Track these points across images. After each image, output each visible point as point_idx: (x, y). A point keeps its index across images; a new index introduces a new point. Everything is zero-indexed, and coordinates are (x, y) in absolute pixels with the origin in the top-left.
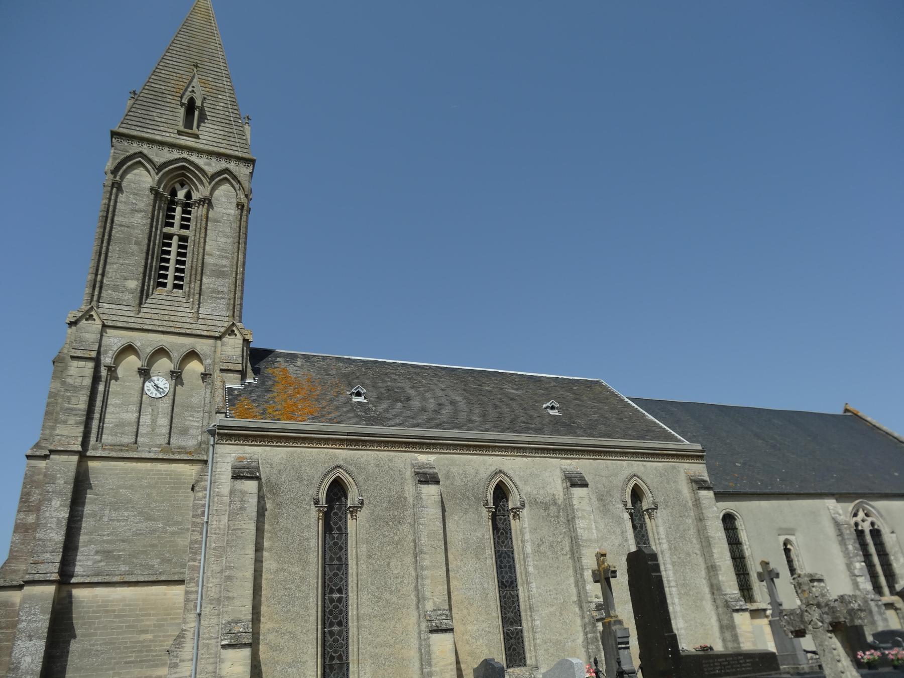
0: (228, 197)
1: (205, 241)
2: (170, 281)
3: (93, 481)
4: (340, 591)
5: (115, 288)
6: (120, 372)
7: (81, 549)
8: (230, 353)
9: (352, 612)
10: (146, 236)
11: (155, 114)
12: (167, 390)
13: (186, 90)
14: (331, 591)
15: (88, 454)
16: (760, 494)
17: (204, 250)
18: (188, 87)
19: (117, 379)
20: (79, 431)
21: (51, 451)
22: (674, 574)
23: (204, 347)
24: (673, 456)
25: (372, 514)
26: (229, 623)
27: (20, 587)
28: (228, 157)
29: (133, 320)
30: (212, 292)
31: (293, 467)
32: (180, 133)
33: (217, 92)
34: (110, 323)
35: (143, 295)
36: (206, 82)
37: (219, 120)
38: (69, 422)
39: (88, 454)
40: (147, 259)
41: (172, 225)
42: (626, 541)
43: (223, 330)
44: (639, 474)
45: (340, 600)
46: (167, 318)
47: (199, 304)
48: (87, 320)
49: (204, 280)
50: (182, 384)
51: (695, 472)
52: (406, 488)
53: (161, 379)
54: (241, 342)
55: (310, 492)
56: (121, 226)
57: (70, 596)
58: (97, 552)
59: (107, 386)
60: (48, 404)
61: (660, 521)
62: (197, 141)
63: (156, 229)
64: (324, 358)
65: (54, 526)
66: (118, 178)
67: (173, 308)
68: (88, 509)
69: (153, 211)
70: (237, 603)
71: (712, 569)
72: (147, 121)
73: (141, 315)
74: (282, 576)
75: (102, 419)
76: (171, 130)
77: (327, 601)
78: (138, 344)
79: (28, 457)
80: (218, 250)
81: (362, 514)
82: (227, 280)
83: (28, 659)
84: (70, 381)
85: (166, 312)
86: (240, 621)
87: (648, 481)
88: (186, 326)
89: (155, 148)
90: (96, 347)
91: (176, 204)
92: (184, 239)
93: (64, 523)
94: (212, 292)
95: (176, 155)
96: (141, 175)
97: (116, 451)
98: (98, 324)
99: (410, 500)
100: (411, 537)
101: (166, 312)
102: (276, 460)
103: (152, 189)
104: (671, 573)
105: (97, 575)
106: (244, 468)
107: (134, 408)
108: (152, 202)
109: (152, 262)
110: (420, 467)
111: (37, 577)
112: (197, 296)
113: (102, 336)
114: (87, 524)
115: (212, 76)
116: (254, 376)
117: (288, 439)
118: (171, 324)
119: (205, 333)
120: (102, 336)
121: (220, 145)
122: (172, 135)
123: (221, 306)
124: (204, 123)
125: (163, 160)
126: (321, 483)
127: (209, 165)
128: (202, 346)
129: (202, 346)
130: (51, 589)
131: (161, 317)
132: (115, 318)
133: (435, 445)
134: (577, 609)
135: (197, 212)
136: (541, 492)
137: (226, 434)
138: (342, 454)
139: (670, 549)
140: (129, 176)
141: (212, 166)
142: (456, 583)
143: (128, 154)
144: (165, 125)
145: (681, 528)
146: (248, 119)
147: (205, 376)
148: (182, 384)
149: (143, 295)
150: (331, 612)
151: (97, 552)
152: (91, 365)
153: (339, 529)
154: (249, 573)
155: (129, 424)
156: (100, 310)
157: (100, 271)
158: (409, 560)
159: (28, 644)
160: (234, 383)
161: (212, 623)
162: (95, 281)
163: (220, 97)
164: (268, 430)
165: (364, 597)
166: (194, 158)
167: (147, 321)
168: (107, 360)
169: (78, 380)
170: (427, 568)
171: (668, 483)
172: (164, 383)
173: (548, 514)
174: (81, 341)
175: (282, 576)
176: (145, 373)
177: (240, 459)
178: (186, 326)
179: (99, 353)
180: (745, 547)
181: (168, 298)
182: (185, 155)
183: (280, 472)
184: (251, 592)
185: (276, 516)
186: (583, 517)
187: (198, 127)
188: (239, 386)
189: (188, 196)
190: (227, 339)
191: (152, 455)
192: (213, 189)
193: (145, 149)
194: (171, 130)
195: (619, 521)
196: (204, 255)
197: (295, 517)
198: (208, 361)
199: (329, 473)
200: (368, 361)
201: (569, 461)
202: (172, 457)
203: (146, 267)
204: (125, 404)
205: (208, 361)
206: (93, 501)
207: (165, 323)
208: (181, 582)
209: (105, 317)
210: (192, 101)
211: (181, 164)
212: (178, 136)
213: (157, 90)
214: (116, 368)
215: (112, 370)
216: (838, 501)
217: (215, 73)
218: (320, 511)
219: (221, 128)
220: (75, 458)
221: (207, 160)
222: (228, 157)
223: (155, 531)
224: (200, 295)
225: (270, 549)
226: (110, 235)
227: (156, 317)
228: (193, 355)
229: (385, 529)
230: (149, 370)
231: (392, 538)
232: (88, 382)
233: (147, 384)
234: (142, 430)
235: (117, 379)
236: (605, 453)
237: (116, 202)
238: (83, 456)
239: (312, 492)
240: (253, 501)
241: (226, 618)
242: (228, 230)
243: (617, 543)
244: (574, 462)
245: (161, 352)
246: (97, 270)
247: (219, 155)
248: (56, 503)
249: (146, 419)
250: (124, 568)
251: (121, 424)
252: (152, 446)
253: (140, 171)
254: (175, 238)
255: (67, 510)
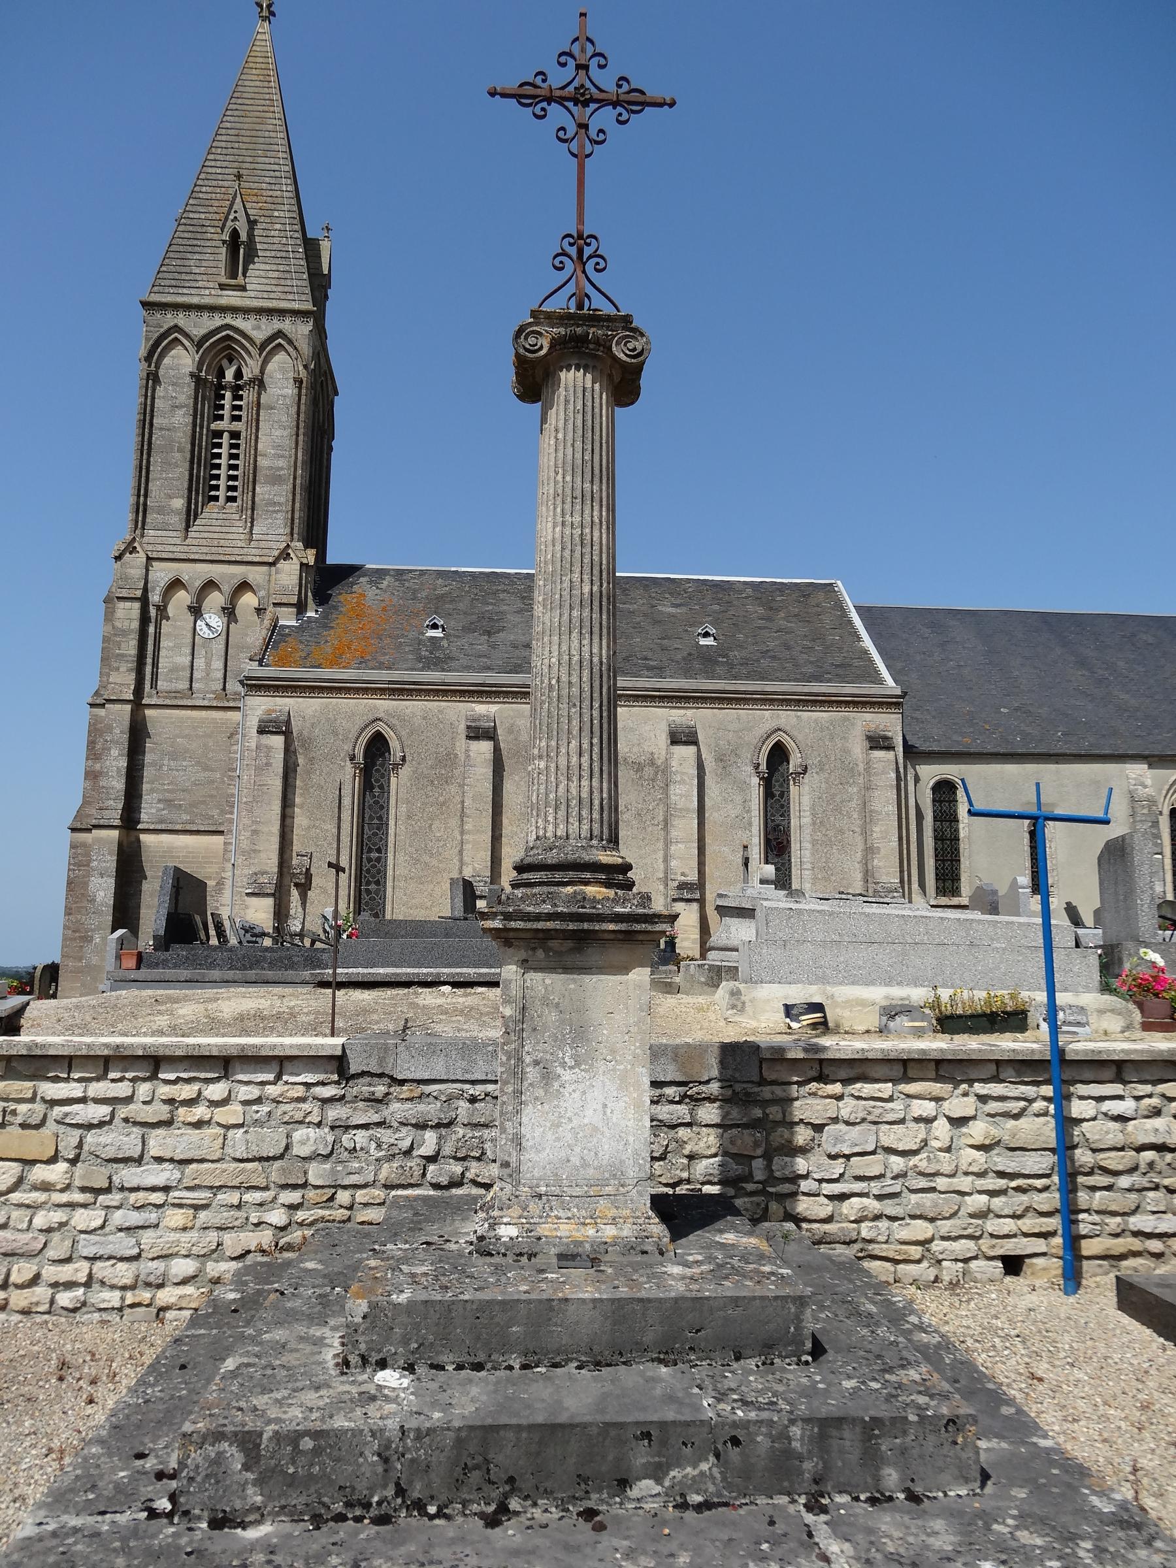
0: (283, 370)
1: (257, 437)
2: (221, 493)
3: (151, 731)
4: (379, 851)
5: (161, 510)
6: (171, 610)
7: (144, 797)
8: (286, 583)
9: (390, 873)
10: (189, 440)
11: (192, 263)
12: (220, 629)
13: (226, 219)
14: (370, 850)
15: (144, 702)
16: (992, 754)
17: (256, 449)
18: (229, 213)
19: (168, 618)
20: (131, 678)
21: (109, 701)
22: (813, 854)
23: (257, 577)
24: (847, 703)
25: (414, 772)
26: (256, 874)
27: (88, 830)
28: (281, 313)
29: (179, 548)
30: (267, 505)
31: (328, 720)
32: (222, 287)
33: (273, 206)
34: (155, 555)
35: (191, 516)
36: (259, 192)
37: (273, 253)
38: (121, 669)
39: (144, 702)
40: (191, 469)
41: (221, 418)
42: (749, 811)
43: (276, 553)
44: (788, 728)
45: (378, 860)
46: (216, 543)
47: (252, 523)
48: (131, 553)
49: (258, 489)
50: (236, 621)
51: (878, 726)
52: (458, 744)
53: (213, 616)
54: (298, 567)
55: (346, 747)
56: (161, 429)
57: (139, 840)
58: (160, 801)
59: (158, 627)
60: (103, 649)
61: (806, 789)
62: (244, 294)
63: (202, 427)
64: (423, 573)
65: (115, 774)
66: (153, 367)
67: (224, 529)
68: (148, 758)
69: (196, 403)
70: (263, 855)
71: (869, 851)
72: (183, 276)
73: (188, 541)
74: (313, 832)
75: (155, 664)
76: (211, 285)
77: (364, 860)
78: (185, 578)
79: (92, 705)
80: (274, 448)
81: (405, 772)
82: (285, 487)
83: (102, 894)
84: (118, 624)
85: (216, 536)
86: (266, 873)
87: (800, 737)
88: (236, 551)
89: (193, 314)
90: (142, 584)
91: (224, 388)
92: (235, 435)
93: (124, 771)
94: (267, 505)
95: (218, 321)
96: (178, 357)
97: (170, 698)
98: (141, 558)
99: (462, 757)
100: (458, 799)
101: (216, 536)
102: (310, 712)
103: (192, 375)
104: (807, 854)
105: (161, 822)
106: (271, 721)
107: (188, 651)
108: (192, 392)
109: (198, 471)
110: (474, 720)
111: (102, 822)
112: (249, 512)
113: (147, 570)
114: (148, 773)
115: (267, 180)
116: (315, 607)
117: (322, 689)
118: (220, 550)
119: (257, 559)
120: (147, 570)
121: (272, 295)
122: (213, 292)
123: (278, 522)
124: (254, 263)
125: (203, 332)
126: (357, 739)
127: (258, 328)
128: (255, 575)
129: (255, 575)
130: (115, 834)
131: (209, 542)
132: (160, 548)
133: (497, 694)
134: (661, 887)
135: (248, 395)
136: (635, 750)
137: (254, 685)
138: (383, 705)
139: (814, 823)
140: (166, 361)
141: (258, 329)
142: (509, 850)
143: (162, 330)
144: (205, 277)
145: (838, 799)
146: (328, 229)
147: (259, 611)
148: (236, 621)
149: (191, 516)
150: (368, 871)
151: (160, 801)
152: (137, 605)
153: (381, 787)
154: (276, 828)
155: (183, 669)
156: (145, 540)
157: (142, 492)
158: (454, 822)
159: (100, 880)
160: (288, 620)
161: (244, 871)
162: (138, 503)
163: (276, 214)
164: (298, 680)
165: (401, 858)
166: (239, 323)
167: (194, 549)
168: (155, 598)
169: (126, 623)
170: (469, 832)
171: (832, 739)
172: (215, 620)
173: (641, 777)
174: (127, 579)
175: (313, 832)
176: (196, 611)
177: (269, 712)
178: (236, 551)
179: (145, 590)
180: (961, 826)
181: (221, 516)
182: (228, 320)
183: (313, 725)
184: (277, 846)
185: (308, 773)
186: (682, 782)
187: (244, 275)
188: (294, 623)
189: (238, 375)
190: (282, 564)
191: (206, 703)
192: (265, 362)
193: (181, 319)
194: (211, 285)
195: (743, 787)
196: (256, 457)
197: (329, 774)
198: (262, 593)
199: (367, 726)
200: (481, 573)
201: (682, 712)
202: (227, 704)
203: (191, 480)
204: (178, 647)
205: (262, 593)
206: (153, 750)
207: (214, 550)
208: (221, 833)
209: (150, 548)
210: (235, 234)
211: (224, 334)
212: (220, 292)
213: (195, 222)
214: (165, 607)
215: (162, 609)
216: (1151, 766)
217: (272, 174)
218: (356, 768)
219: (275, 267)
220: (128, 707)
221: (255, 322)
222: (281, 313)
223: (213, 782)
224: (253, 509)
225: (301, 807)
226: (150, 443)
227: (204, 542)
228: (244, 586)
229: (429, 788)
230: (200, 607)
231: (437, 799)
232: (135, 625)
233: (199, 623)
234: (196, 675)
235: (168, 618)
236: (738, 701)
237: (153, 398)
238: (137, 703)
239: (348, 747)
240: (278, 758)
241: (253, 870)
242: (284, 419)
243: (733, 814)
244: (689, 713)
245: (210, 585)
246: (139, 490)
247: (270, 312)
248: (115, 752)
249: (200, 663)
250: (185, 817)
251: (175, 669)
252: (207, 692)
253: (178, 351)
254: (226, 435)
255: (125, 759)
